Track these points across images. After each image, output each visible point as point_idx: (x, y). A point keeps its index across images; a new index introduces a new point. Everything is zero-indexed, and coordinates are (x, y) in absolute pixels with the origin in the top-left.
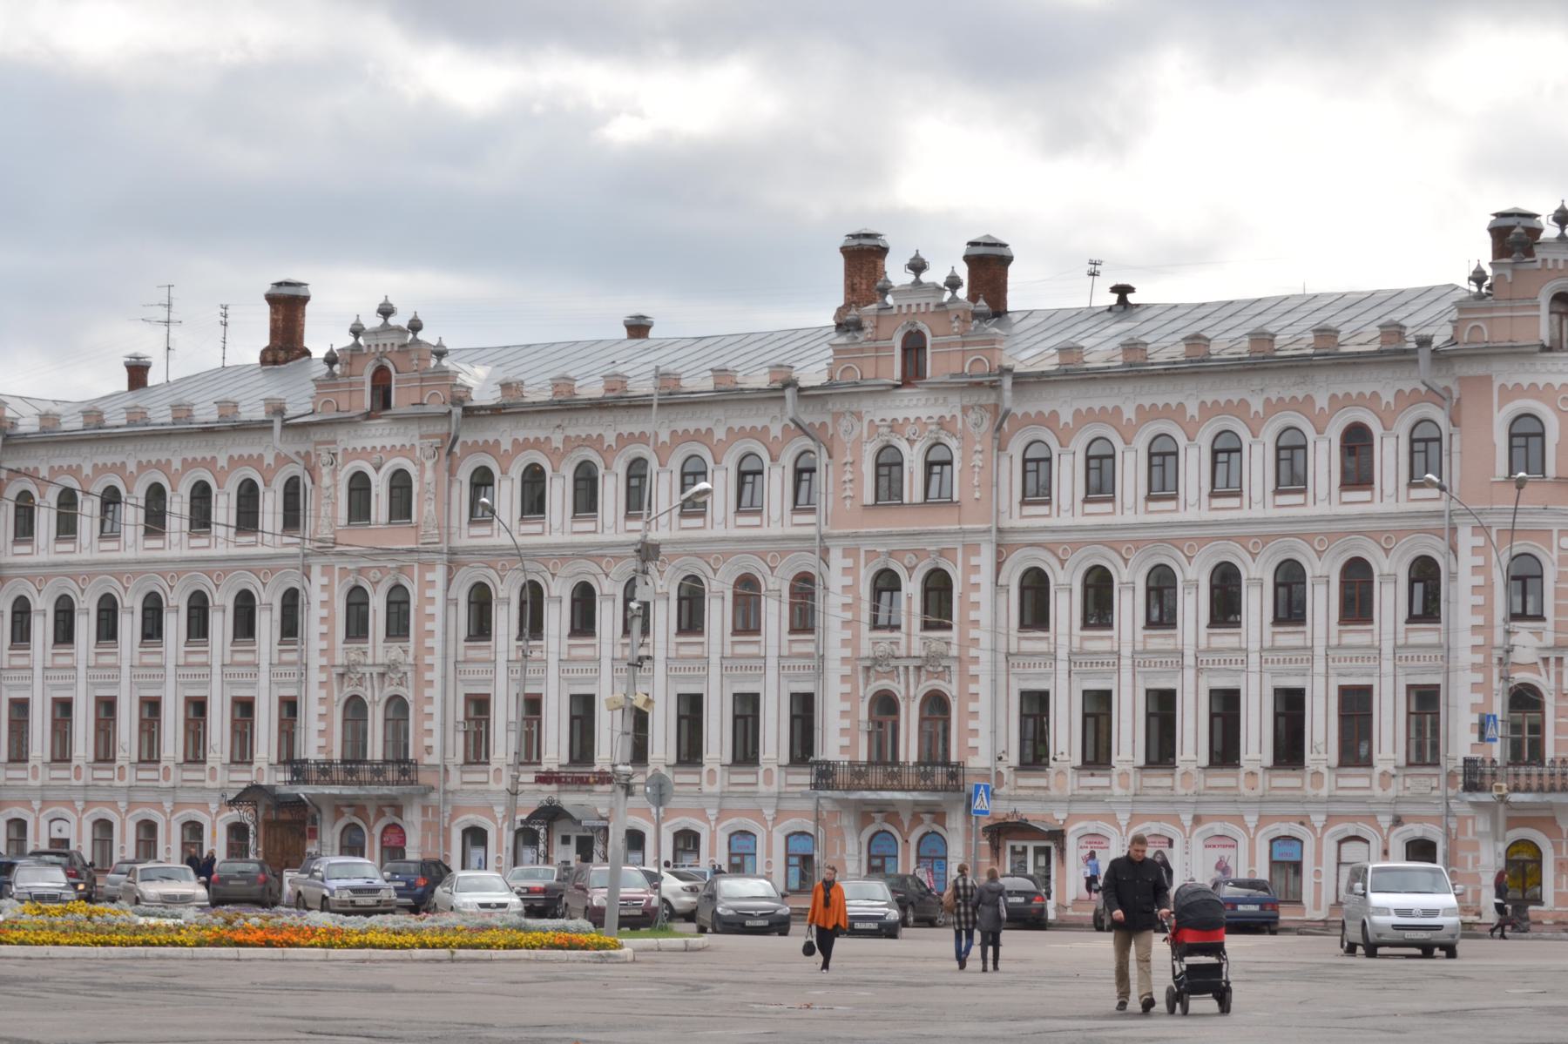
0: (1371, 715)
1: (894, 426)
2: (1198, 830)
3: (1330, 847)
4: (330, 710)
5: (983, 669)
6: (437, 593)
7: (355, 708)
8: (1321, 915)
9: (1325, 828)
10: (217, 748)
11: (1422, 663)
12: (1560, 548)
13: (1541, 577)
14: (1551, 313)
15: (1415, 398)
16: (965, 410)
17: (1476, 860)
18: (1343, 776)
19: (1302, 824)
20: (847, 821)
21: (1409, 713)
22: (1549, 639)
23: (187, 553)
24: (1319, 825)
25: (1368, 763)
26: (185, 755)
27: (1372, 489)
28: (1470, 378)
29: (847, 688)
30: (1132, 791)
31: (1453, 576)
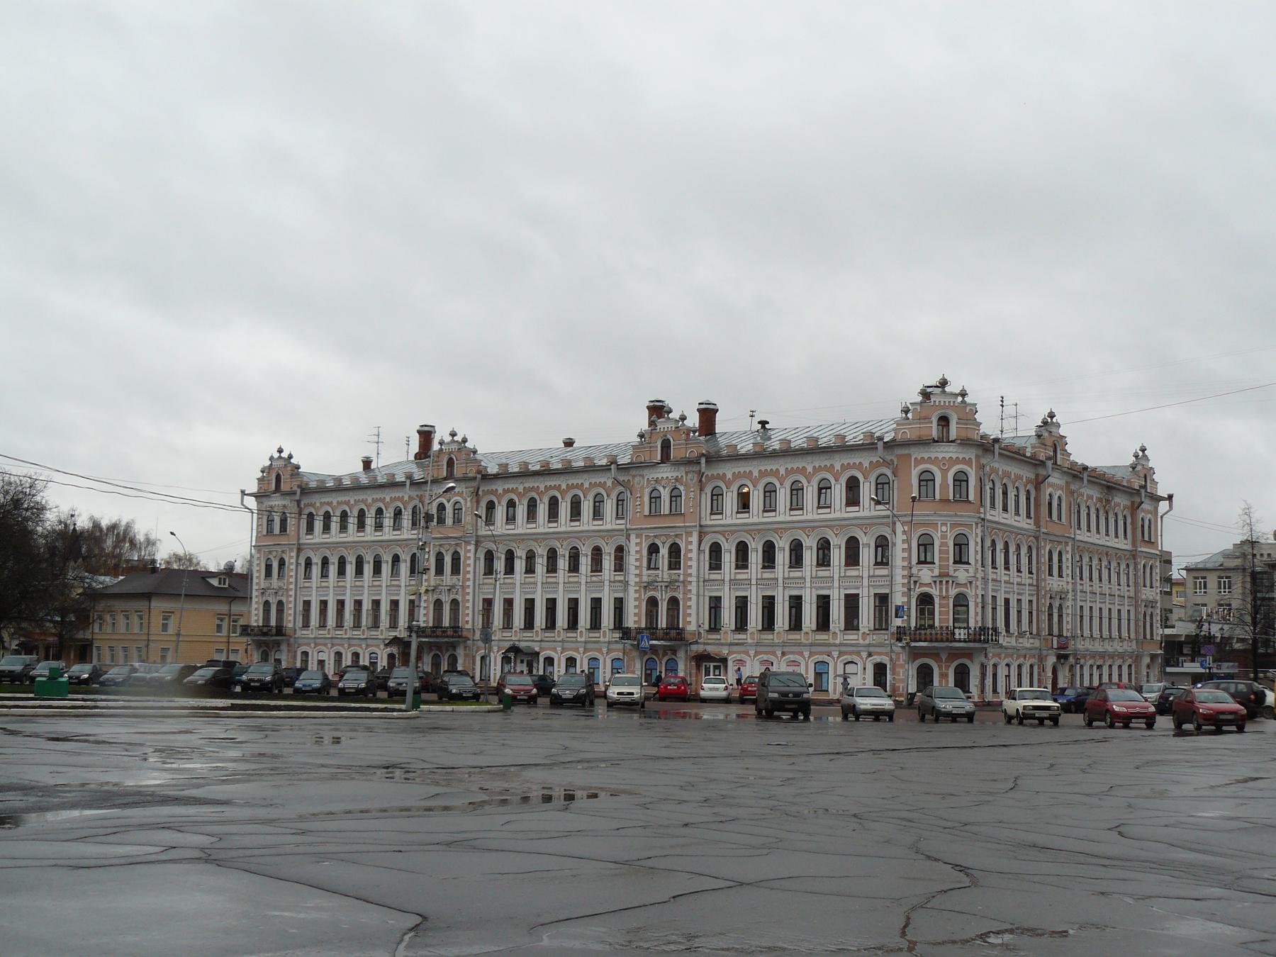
0: (846, 608)
1: (657, 481)
5: (693, 587)
6: (471, 555)
7: (926, 601)
15: (878, 465)
16: (687, 473)
20: (903, 657)
22: (936, 572)
31: (894, 544)
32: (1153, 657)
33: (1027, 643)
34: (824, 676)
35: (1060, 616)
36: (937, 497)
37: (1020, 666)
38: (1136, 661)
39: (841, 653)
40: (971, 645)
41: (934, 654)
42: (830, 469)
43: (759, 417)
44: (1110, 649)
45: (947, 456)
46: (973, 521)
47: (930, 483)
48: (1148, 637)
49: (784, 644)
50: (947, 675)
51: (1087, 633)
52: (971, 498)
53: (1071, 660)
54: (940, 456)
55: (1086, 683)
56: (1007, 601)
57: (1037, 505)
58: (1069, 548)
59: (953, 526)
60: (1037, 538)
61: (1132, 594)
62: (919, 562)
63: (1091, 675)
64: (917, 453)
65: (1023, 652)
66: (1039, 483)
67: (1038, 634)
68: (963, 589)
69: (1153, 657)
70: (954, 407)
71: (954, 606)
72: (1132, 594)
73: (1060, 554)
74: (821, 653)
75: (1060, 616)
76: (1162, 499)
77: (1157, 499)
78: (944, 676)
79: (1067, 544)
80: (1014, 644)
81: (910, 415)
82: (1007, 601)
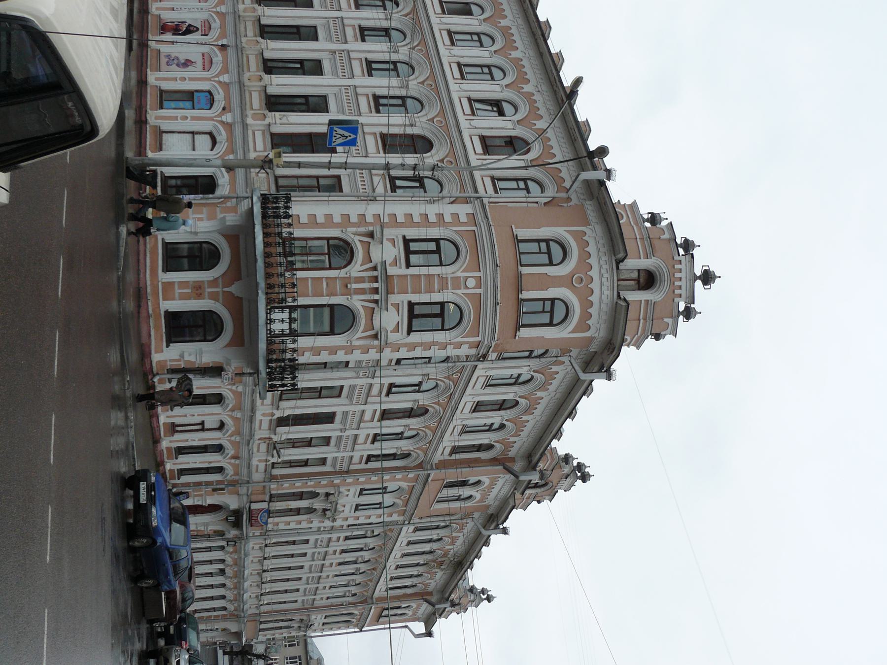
3: (207, 126)
4: (337, 225)
7: (341, 251)
8: (152, 44)
9: (222, 122)
10: (284, 120)
11: (361, 187)
12: (466, 278)
14: (639, 270)
17: (200, 219)
18: (263, 134)
19: (224, 109)
20: (232, 219)
22: (391, 271)
23: (455, 97)
24: (224, 118)
27: (484, 154)
28: (585, 213)
29: (354, 219)
30: (241, 14)
32: (238, 635)
33: (259, 458)
34: (188, 104)
35: (298, 511)
36: (525, 270)
37: (219, 448)
38: (232, 615)
39: (229, 126)
40: (262, 346)
41: (241, 269)
42: (534, 113)
44: (246, 584)
45: (595, 286)
46: (484, 337)
47: (544, 259)
48: (262, 626)
49: (239, 50)
50: (199, 296)
51: (271, 551)
52: (524, 333)
53: (233, 533)
54: (594, 273)
56: (329, 418)
57: (470, 463)
58: (395, 517)
59: (477, 300)
60: (420, 466)
61: (317, 603)
62: (407, 242)
63: (210, 562)
64: (594, 234)
65: (244, 454)
66: (503, 462)
67: (273, 478)
68: (362, 321)
69: (238, 635)
70: (673, 298)
71: (332, 307)
72: (317, 603)
74: (228, 98)
75: (298, 511)
77: (429, 622)
78: (198, 290)
79: (403, 513)
80: (259, 434)
82: (329, 418)
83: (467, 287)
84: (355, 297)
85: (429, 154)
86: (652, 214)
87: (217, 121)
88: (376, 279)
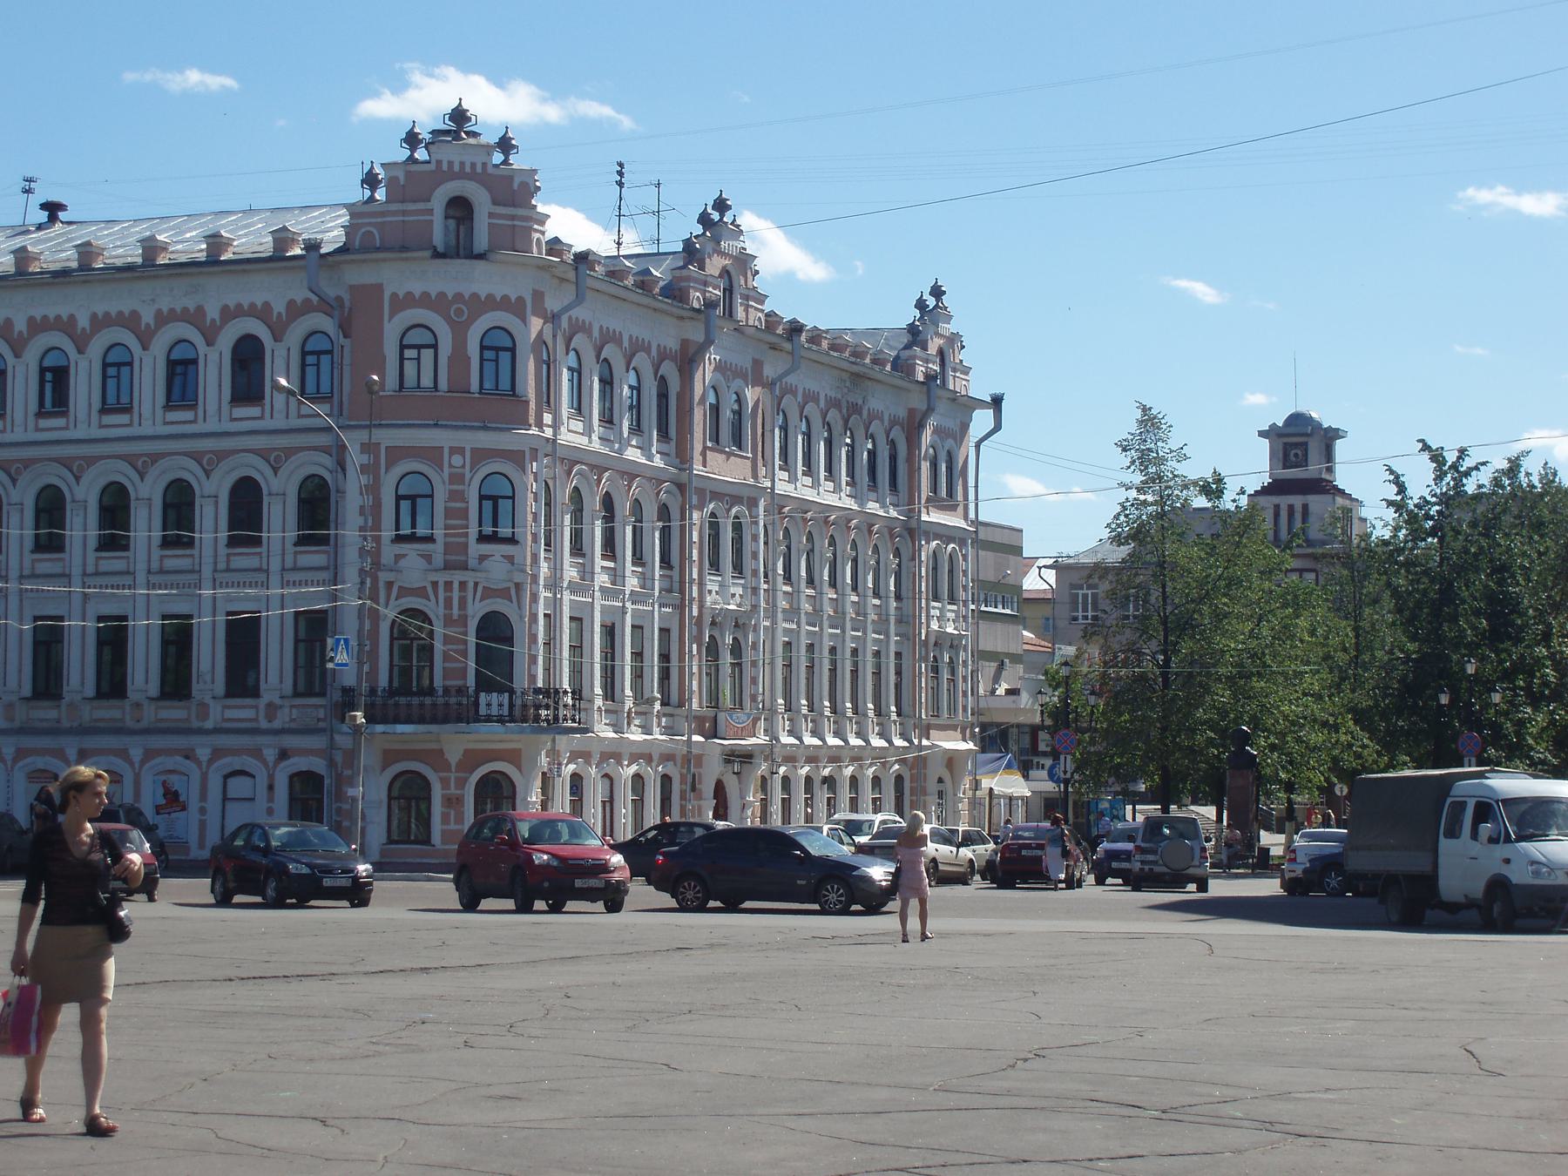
0: (229, 644)
2: (283, 764)
9: (211, 762)
10: (208, 678)
13: (432, 496)
14: (446, 218)
18: (229, 707)
19: (187, 757)
21: (297, 641)
25: (256, 693)
26: (295, 685)
43: (43, 194)
55: (652, 817)
73: (737, 527)
76: (981, 404)
81: (380, 195)
83: (463, 466)
84: (470, 611)
85: (263, 485)
86: (363, 182)
87: (209, 766)
88: (449, 585)
